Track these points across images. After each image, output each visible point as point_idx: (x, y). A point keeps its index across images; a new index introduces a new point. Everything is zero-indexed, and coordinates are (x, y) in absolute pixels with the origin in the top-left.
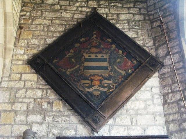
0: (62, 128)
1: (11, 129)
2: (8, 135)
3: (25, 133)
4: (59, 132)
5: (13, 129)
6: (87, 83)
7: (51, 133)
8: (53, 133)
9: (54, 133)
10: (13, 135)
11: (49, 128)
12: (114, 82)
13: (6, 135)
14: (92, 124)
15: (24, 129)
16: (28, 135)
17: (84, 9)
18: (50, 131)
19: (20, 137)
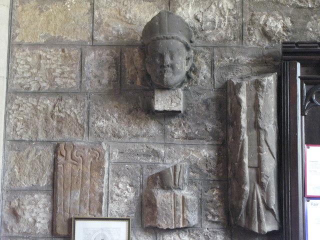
0: (301, 7)
1: (87, 18)
2: (80, 38)
3: (152, 28)
4: (290, 24)
5: (96, 13)
6: (256, 141)
7: (256, 32)
8: (263, 29)
9: (267, 29)
10: (100, 38)
11: (246, 10)
12: (313, 15)
13: (73, 39)
14: (89, 135)
15: (143, 16)
16: (168, 35)
17: (278, 7)
18: (252, 22)
19: (128, 46)
